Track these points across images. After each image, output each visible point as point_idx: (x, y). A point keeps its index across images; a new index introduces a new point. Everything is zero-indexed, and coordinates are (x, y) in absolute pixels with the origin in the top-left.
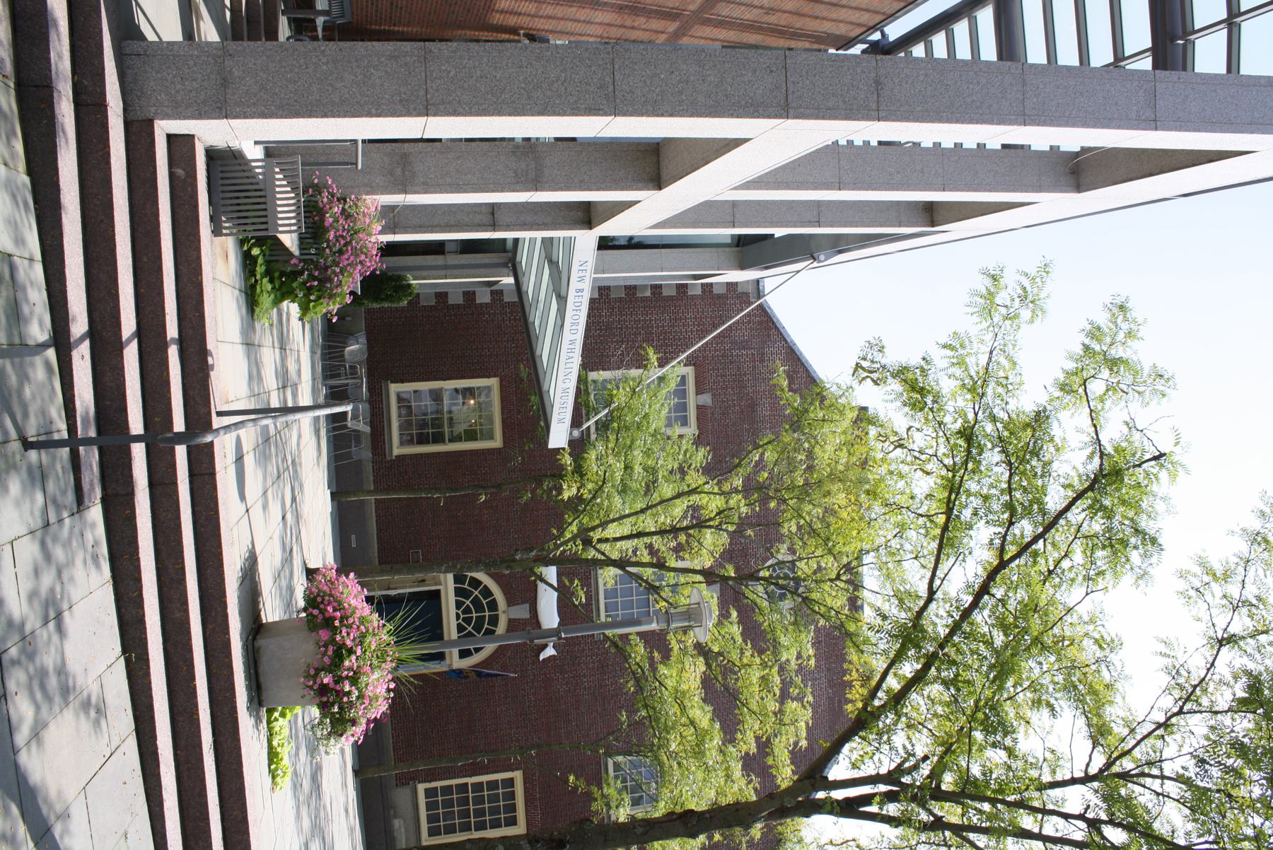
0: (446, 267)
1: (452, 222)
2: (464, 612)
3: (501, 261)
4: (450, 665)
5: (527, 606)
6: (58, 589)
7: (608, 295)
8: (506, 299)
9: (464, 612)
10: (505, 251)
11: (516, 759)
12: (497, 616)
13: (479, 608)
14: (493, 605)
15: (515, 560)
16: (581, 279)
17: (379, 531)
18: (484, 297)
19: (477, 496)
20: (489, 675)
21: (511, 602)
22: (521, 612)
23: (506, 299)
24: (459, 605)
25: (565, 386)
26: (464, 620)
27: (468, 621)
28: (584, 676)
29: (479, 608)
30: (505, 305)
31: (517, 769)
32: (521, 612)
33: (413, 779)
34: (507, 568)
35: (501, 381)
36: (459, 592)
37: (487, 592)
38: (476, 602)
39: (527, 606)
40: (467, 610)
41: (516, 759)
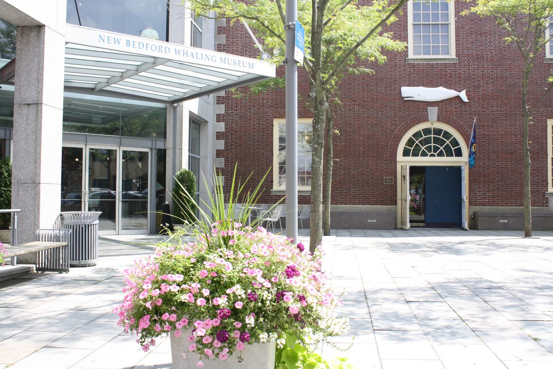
0: (174, 149)
1: (34, 137)
2: (430, 151)
3: (172, 111)
4: (466, 163)
5: (429, 108)
6: (459, 336)
7: (224, 46)
8: (223, 112)
9: (430, 151)
10: (166, 109)
11: (532, 120)
12: (434, 129)
13: (427, 141)
14: (427, 131)
15: (316, 97)
16: (117, 41)
17: (369, 203)
18: (221, 127)
19: (335, 136)
20: (474, 138)
21: (425, 119)
22: (433, 112)
23: (223, 112)
24: (424, 154)
25: (218, 60)
26: (435, 152)
27: (436, 149)
28: (483, 72)
29: (442, 143)
30: (227, 114)
31: (546, 122)
32: (433, 112)
33: (544, 195)
34: (321, 104)
35: (276, 117)
36: (415, 154)
37: (417, 135)
38: (423, 142)
39: (429, 108)
40: (429, 149)
41: (532, 120)
